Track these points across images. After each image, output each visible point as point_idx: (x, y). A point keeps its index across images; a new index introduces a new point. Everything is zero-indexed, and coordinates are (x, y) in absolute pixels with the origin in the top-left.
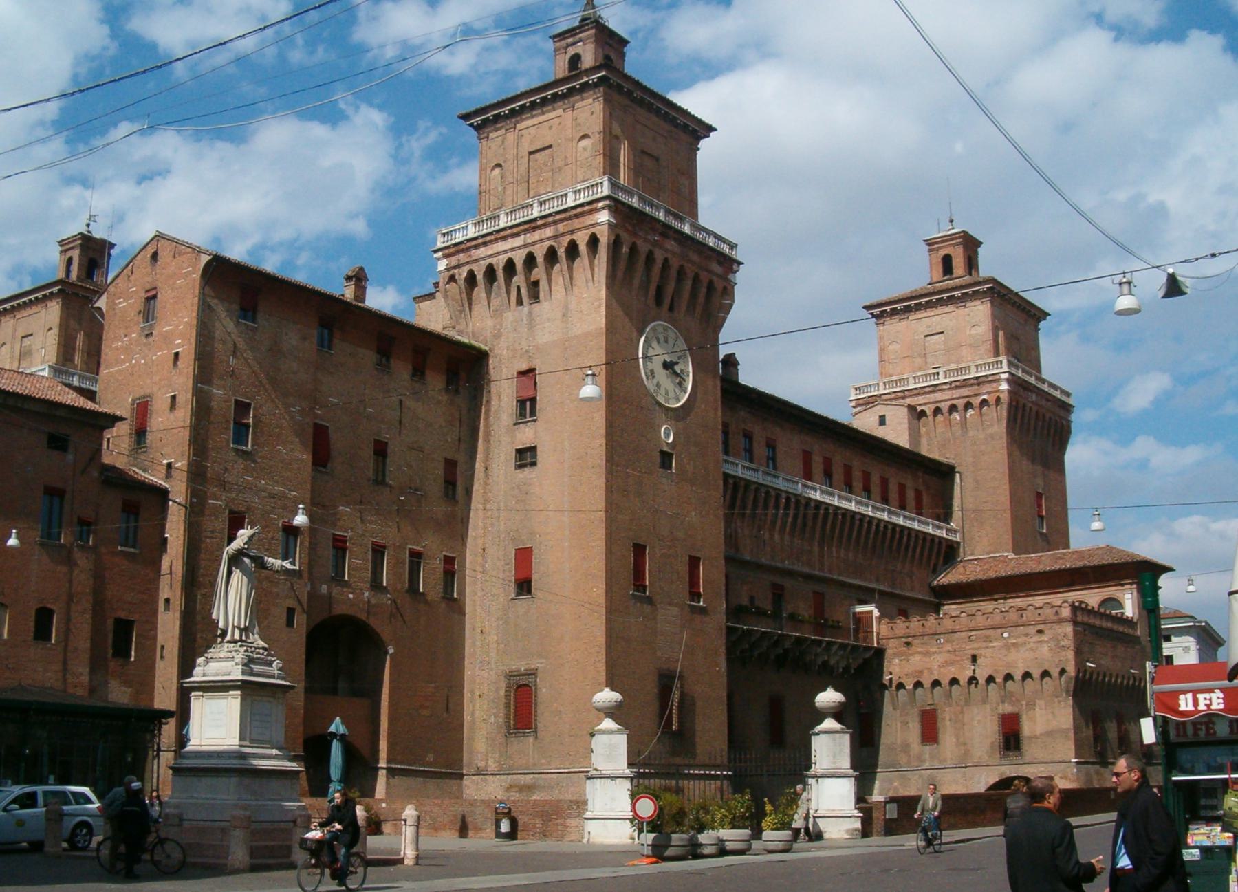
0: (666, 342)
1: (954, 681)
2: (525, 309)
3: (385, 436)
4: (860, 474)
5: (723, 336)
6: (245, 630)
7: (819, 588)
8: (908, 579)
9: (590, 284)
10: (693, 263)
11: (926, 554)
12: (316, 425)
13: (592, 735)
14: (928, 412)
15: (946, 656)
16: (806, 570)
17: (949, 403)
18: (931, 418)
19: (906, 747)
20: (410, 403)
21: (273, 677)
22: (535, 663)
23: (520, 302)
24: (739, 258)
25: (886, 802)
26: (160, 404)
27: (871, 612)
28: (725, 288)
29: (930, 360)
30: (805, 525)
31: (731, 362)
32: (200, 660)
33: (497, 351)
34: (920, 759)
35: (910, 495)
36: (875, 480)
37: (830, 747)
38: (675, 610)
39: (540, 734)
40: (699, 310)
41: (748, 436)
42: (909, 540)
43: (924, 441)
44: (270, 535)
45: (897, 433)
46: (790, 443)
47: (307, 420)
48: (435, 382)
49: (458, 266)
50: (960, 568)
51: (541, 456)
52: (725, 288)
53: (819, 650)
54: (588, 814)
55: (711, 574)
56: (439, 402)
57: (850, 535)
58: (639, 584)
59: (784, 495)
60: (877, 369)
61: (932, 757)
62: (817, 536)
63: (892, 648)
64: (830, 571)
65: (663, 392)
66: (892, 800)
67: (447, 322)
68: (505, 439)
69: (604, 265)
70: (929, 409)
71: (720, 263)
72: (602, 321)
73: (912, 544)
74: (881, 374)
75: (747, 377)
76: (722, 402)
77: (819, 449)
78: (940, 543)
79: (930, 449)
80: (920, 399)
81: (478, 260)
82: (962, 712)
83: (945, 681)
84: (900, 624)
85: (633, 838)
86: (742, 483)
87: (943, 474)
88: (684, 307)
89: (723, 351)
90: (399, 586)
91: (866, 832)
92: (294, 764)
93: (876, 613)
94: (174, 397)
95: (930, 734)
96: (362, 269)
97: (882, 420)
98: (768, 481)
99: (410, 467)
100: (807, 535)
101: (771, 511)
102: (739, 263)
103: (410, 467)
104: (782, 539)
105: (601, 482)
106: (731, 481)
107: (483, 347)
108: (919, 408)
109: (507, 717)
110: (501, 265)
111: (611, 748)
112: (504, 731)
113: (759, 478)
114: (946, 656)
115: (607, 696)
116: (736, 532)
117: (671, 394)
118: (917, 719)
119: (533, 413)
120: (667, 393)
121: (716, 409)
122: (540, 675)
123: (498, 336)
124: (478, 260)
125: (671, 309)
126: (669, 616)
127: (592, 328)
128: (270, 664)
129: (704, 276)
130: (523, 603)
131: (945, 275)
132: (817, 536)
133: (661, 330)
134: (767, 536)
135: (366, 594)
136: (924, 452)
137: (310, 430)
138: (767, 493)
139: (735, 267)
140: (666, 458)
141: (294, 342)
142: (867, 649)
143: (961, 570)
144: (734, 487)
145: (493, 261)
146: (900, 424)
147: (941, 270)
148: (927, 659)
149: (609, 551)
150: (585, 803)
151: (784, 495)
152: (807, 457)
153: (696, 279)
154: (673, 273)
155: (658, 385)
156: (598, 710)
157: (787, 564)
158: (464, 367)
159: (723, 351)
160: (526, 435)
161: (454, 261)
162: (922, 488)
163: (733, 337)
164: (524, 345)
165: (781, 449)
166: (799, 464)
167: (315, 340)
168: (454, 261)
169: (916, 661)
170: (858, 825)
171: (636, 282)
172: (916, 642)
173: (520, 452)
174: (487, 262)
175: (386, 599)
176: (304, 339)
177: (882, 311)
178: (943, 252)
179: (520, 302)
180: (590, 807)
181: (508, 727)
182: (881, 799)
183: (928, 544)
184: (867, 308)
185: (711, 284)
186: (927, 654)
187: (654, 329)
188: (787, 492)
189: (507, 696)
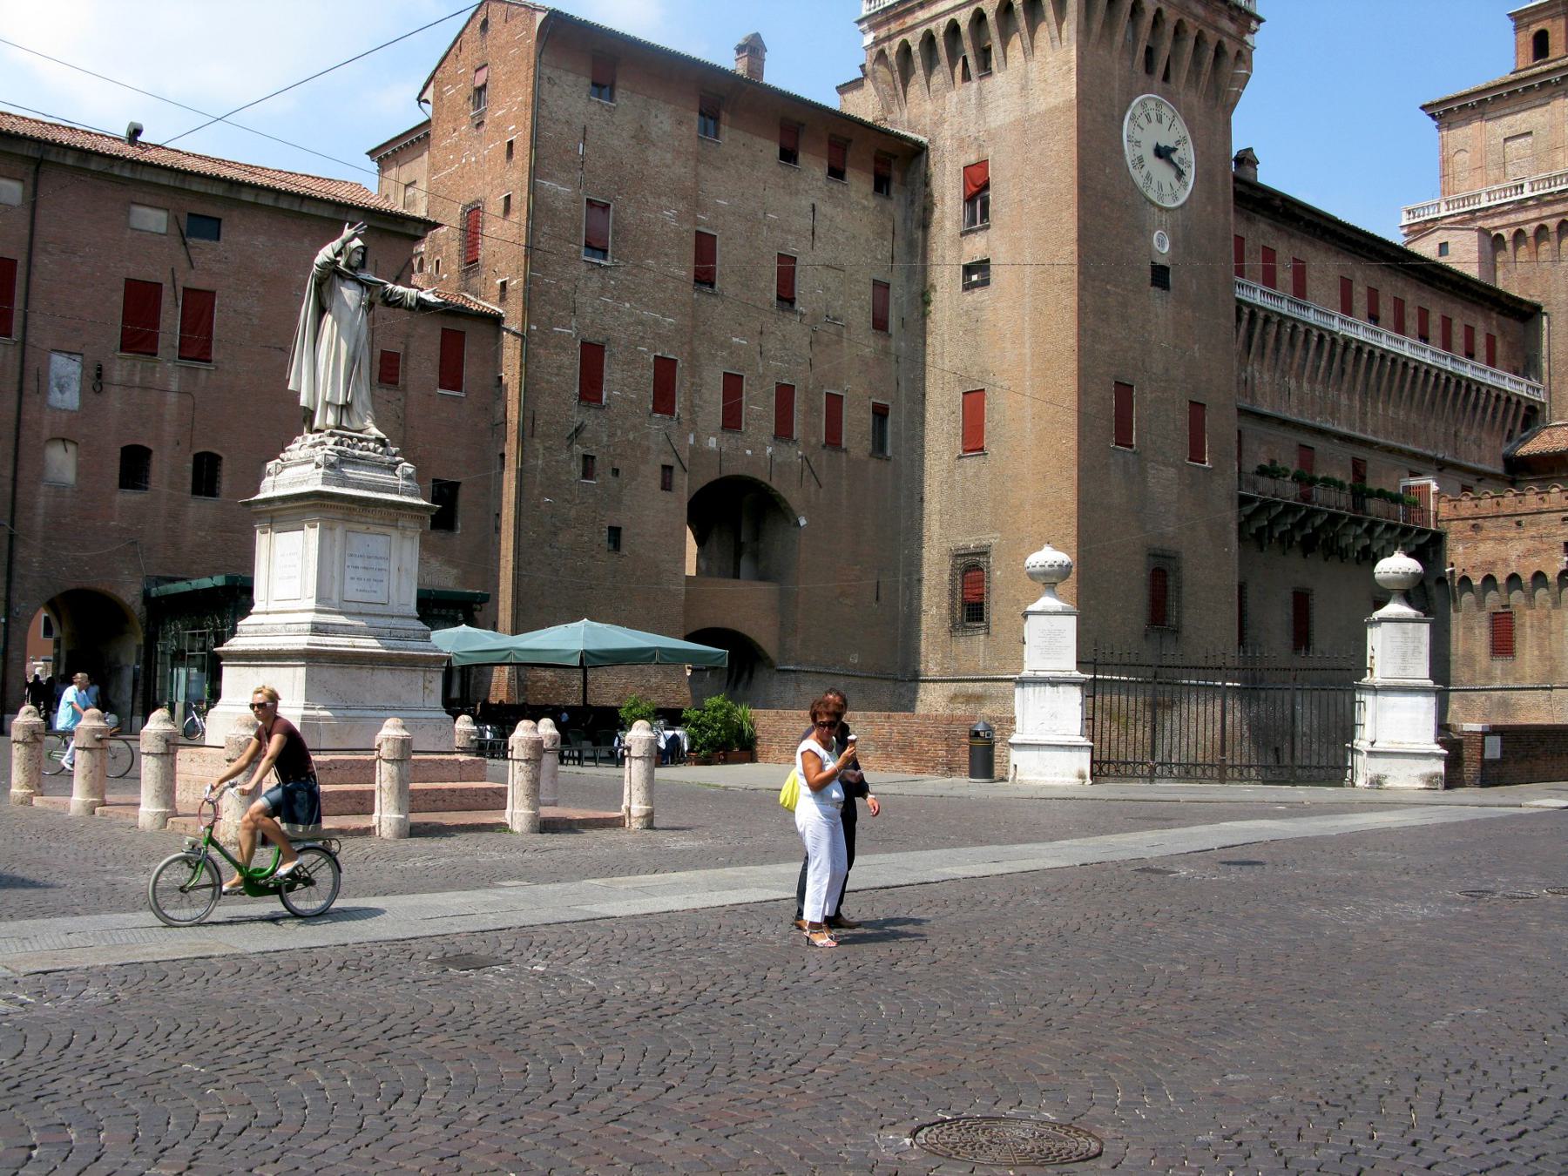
0: (1160, 121)
1: (1539, 577)
2: (974, 85)
3: (790, 250)
4: (1416, 311)
5: (1238, 118)
6: (346, 408)
7: (1361, 453)
8: (1474, 447)
9: (1057, 43)
10: (1196, 17)
11: (1500, 415)
12: (698, 233)
13: (1025, 615)
14: (1506, 237)
15: (1530, 543)
16: (1344, 430)
17: (1535, 224)
18: (1510, 246)
19: (1470, 659)
20: (824, 208)
21: (395, 490)
22: (988, 538)
23: (966, 77)
24: (1259, 12)
25: (1484, 734)
26: (494, 206)
27: (1428, 486)
28: (1239, 54)
29: (1510, 169)
30: (1343, 371)
31: (1246, 159)
32: (270, 466)
33: (939, 143)
34: (1489, 675)
35: (1480, 341)
36: (1435, 319)
37: (1394, 645)
38: (1171, 472)
39: (993, 629)
40: (1204, 80)
41: (1269, 254)
42: (1477, 398)
43: (1500, 274)
44: (637, 373)
45: (1464, 256)
46: (1325, 267)
47: (687, 227)
48: (859, 184)
49: (889, 38)
50: (1545, 435)
51: (996, 273)
52: (1239, 54)
53: (1359, 531)
54: (1014, 739)
55: (1221, 425)
56: (864, 208)
57: (1402, 387)
58: (1123, 435)
59: (1315, 332)
60: (1438, 186)
61: (1505, 674)
62: (1359, 387)
63: (1454, 531)
64: (1375, 433)
65: (1154, 185)
66: (1494, 730)
67: (878, 114)
68: (950, 255)
69: (1074, 26)
70: (1507, 234)
71: (1232, 19)
72: (1072, 91)
73: (1482, 402)
74: (1443, 193)
75: (1268, 176)
76: (1236, 211)
77: (1363, 276)
78: (1518, 402)
79: (1509, 282)
80: (1497, 222)
81: (912, 28)
82: (1549, 617)
83: (1526, 577)
84: (1467, 506)
85: (1082, 776)
86: (1262, 314)
87: (1525, 314)
88: (1184, 75)
89: (1236, 147)
90: (813, 440)
91: (1453, 778)
92: (374, 643)
93: (1434, 487)
94: (508, 198)
95: (1503, 642)
96: (757, 37)
97: (1443, 247)
98: (1296, 313)
99: (827, 289)
100: (1345, 386)
101: (1299, 352)
102: (1260, 21)
103: (827, 289)
104: (1313, 390)
105: (1072, 301)
106: (1246, 310)
107: (921, 138)
108: (1494, 233)
109: (952, 608)
110: (942, 31)
111: (1050, 637)
112: (948, 624)
113: (1284, 308)
114: (1530, 543)
115: (1048, 556)
116: (1253, 378)
117: (1167, 189)
118: (1486, 624)
119: (985, 214)
120: (1160, 187)
121: (1227, 213)
122: (993, 553)
123: (938, 123)
124: (912, 28)
125: (1166, 78)
126: (1164, 480)
127: (1061, 99)
128: (392, 468)
129: (1211, 37)
130: (972, 464)
131: (1536, 58)
132: (1359, 387)
133: (1151, 105)
134: (1293, 384)
135: (769, 450)
136: (1500, 286)
137: (692, 240)
138: (1294, 327)
139: (1253, 25)
140: (1160, 276)
141: (667, 127)
142: (1422, 532)
143: (1547, 438)
144: (1248, 315)
145: (932, 26)
146: (1469, 251)
147: (1531, 52)
148: (1502, 547)
149: (1083, 392)
150: (1012, 721)
151: (1315, 332)
152: (1346, 286)
153: (1200, 39)
154: (1169, 29)
155: (1148, 177)
156: (1032, 576)
157: (1318, 422)
158: (895, 163)
159: (1236, 147)
160: (976, 247)
161: (883, 32)
162: (1495, 332)
163: (1248, 127)
164: (972, 129)
165: (1312, 274)
166: (1337, 296)
167: (696, 126)
168: (883, 32)
169: (1487, 549)
170: (1439, 767)
171: (1119, 39)
172: (1487, 524)
173: (968, 270)
174: (924, 28)
175: (794, 454)
176: (680, 123)
177: (1446, 113)
178: (1535, 28)
179: (966, 77)
180: (1018, 726)
181: (953, 619)
182: (1476, 727)
183: (1502, 403)
184: (1423, 108)
185: (1220, 46)
186: (1502, 540)
187: (1143, 104)
188: (1318, 328)
189: (952, 581)
